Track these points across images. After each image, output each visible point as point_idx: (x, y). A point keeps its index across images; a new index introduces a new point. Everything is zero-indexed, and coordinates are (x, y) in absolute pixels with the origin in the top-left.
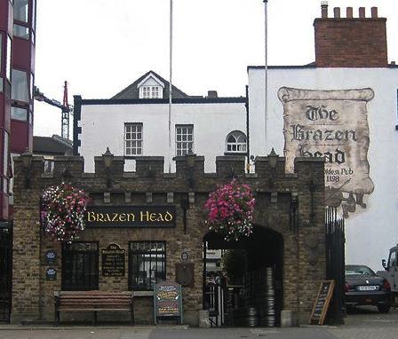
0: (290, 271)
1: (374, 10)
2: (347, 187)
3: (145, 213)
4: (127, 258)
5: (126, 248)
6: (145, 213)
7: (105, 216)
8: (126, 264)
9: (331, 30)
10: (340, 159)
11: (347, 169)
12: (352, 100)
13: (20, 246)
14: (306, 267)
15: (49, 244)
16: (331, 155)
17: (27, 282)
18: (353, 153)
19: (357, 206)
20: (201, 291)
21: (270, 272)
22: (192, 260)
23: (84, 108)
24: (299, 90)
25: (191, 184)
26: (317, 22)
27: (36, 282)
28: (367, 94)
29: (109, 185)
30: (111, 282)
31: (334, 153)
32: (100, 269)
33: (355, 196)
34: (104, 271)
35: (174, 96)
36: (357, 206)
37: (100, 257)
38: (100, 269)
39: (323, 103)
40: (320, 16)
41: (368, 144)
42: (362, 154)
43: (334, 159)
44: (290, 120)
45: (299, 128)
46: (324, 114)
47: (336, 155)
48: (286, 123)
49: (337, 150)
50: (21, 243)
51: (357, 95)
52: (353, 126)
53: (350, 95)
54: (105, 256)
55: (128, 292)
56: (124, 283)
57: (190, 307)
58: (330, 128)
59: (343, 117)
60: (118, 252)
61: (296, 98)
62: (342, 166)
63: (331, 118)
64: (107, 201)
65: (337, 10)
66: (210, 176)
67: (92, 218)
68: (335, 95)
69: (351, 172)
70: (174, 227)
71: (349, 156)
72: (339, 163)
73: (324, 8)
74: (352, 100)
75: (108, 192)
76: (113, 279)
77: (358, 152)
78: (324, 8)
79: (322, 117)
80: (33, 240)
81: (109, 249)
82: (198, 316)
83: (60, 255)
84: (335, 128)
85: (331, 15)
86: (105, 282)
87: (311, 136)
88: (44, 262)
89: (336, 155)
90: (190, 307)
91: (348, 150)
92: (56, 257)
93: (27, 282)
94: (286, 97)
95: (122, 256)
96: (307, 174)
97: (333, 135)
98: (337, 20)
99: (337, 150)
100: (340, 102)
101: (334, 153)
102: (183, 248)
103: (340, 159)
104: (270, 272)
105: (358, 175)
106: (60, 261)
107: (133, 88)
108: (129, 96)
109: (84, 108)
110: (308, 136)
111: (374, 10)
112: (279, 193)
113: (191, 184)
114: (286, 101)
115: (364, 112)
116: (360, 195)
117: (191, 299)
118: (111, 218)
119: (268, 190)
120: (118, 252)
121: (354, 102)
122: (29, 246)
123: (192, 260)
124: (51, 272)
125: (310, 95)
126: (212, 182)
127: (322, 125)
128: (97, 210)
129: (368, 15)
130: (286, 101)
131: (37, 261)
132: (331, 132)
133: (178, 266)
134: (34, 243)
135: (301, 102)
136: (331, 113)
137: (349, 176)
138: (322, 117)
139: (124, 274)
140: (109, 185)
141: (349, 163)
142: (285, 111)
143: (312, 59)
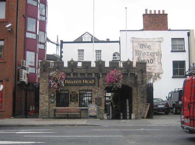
0: (134, 100)
1: (163, 11)
2: (155, 71)
3: (85, 80)
4: (78, 96)
5: (78, 92)
6: (85, 80)
7: (71, 82)
8: (78, 98)
9: (149, 18)
10: (152, 62)
11: (154, 65)
12: (156, 42)
13: (42, 92)
14: (140, 99)
15: (52, 91)
16: (149, 61)
17: (44, 104)
18: (156, 60)
19: (157, 78)
20: (104, 107)
21: (127, 101)
22: (101, 97)
23: (64, 44)
24: (138, 38)
25: (101, 70)
26: (144, 15)
27: (47, 104)
28: (161, 40)
29: (72, 71)
30: (73, 104)
31: (149, 60)
32: (69, 99)
33: (157, 75)
34: (71, 100)
35: (95, 41)
36: (157, 78)
37: (69, 95)
38: (69, 99)
39: (146, 43)
40: (145, 13)
41: (161, 57)
42: (159, 60)
43: (149, 62)
44: (135, 49)
45: (137, 52)
46: (146, 47)
47: (150, 60)
48: (133, 50)
49: (151, 59)
50: (42, 91)
51: (157, 40)
52: (156, 51)
53: (155, 40)
54: (71, 95)
55: (79, 108)
56: (78, 104)
57: (100, 112)
58: (148, 51)
59: (152, 48)
60: (75, 94)
61: (137, 41)
62: (152, 64)
63: (149, 48)
64: (72, 76)
65: (151, 11)
66: (107, 68)
67: (66, 82)
68: (150, 40)
69: (155, 66)
70: (95, 85)
71: (155, 61)
72: (151, 63)
73: (146, 10)
74: (156, 42)
75: (72, 73)
76: (74, 103)
77: (158, 60)
78: (146, 10)
79: (145, 47)
80: (46, 90)
81: (72, 93)
82: (103, 116)
83: (56, 95)
84: (150, 52)
85: (148, 13)
86: (71, 104)
87: (142, 54)
88: (50, 97)
89: (150, 60)
90: (100, 112)
91: (154, 59)
92: (54, 95)
93: (44, 104)
94: (133, 41)
95: (77, 95)
96: (141, 67)
97: (149, 54)
98: (151, 15)
99: (151, 59)
100: (152, 42)
101: (149, 60)
102: (98, 92)
103: (152, 62)
104: (127, 101)
105: (158, 67)
106: (55, 97)
107: (81, 38)
108: (79, 41)
109: (64, 44)
110: (141, 54)
111: (163, 11)
112: (131, 74)
113: (101, 70)
114: (133, 42)
115: (160, 46)
116: (159, 75)
117: (101, 110)
118: (73, 82)
119: (127, 73)
120: (75, 94)
121: (156, 42)
122: (45, 92)
123: (101, 97)
124: (53, 101)
125: (141, 40)
126: (108, 70)
127: (145, 50)
128: (68, 79)
129: (161, 13)
130: (133, 42)
131: (48, 97)
132: (148, 53)
133: (96, 99)
134: (47, 91)
135: (138, 43)
136: (148, 46)
137: (155, 68)
138: (145, 47)
139: (77, 101)
140: (72, 71)
141: (155, 63)
142: (133, 45)
143: (142, 28)
